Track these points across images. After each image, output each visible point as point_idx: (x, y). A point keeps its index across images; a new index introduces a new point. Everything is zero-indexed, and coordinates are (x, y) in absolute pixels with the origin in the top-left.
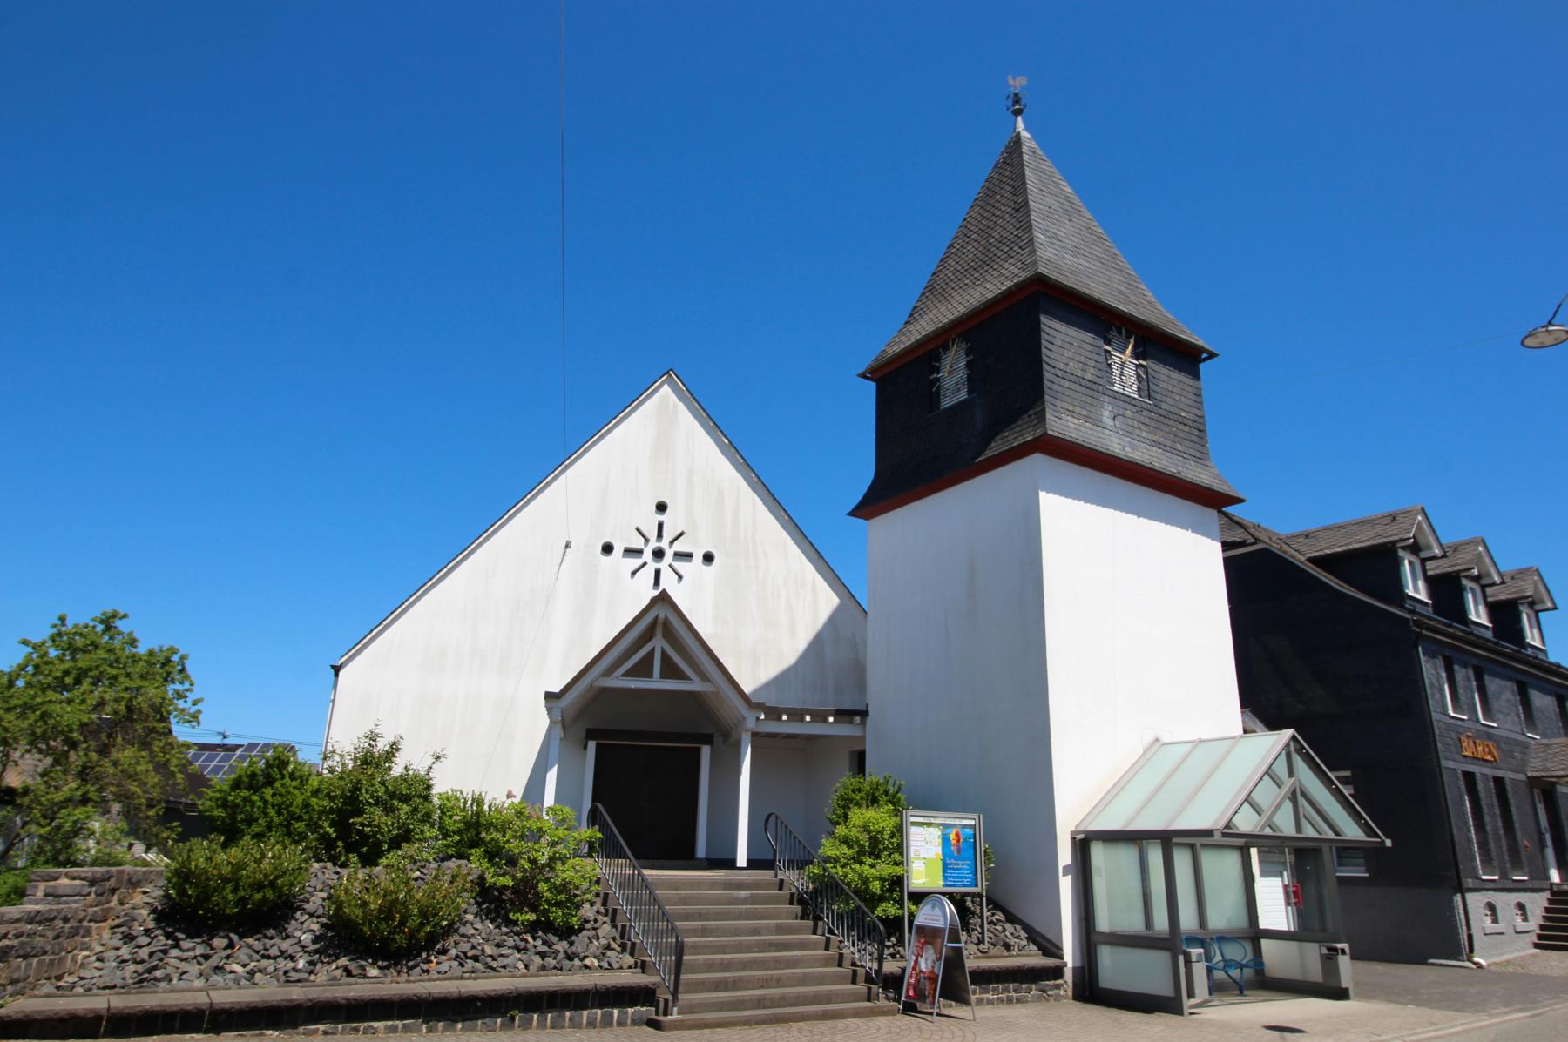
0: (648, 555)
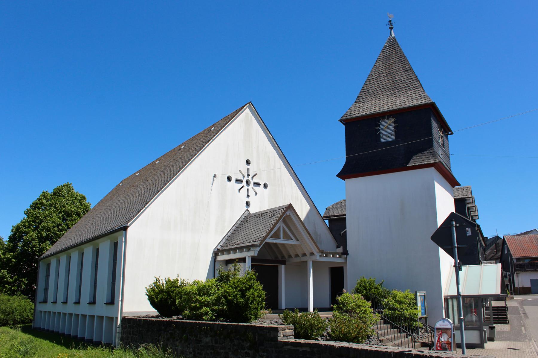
0: (244, 183)
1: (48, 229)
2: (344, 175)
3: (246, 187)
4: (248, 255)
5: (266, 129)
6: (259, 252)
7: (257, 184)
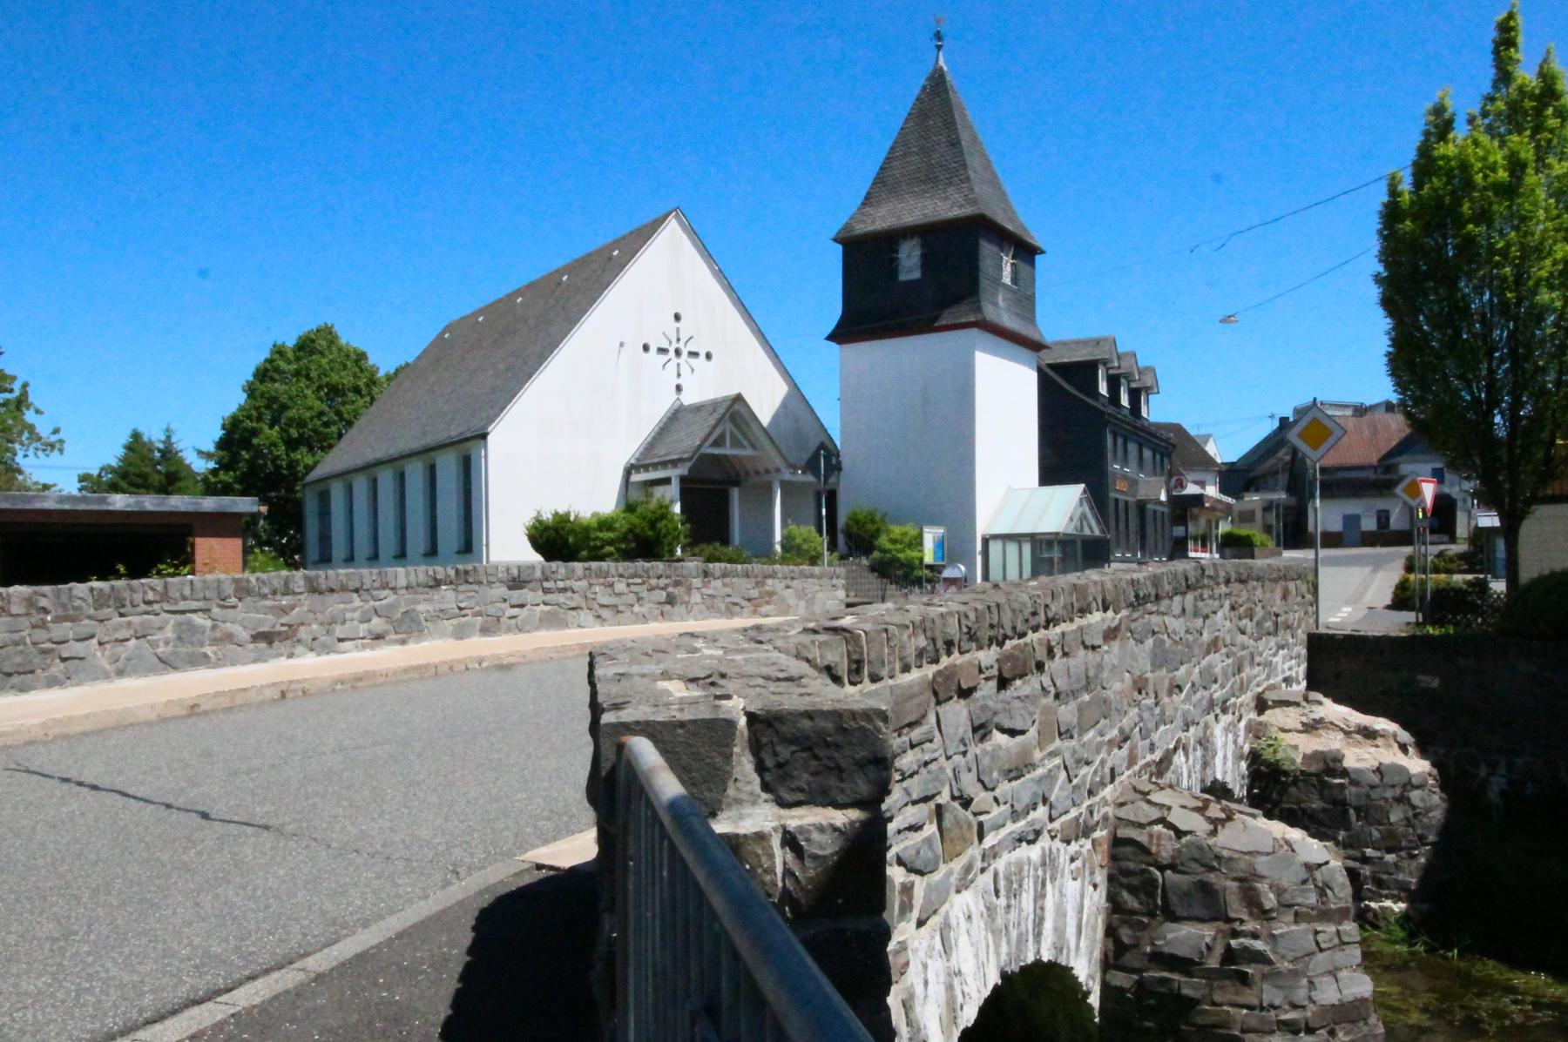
0: (672, 353)
1: (301, 424)
2: (842, 334)
3: (675, 360)
4: (674, 473)
5: (708, 255)
6: (691, 470)
7: (694, 354)
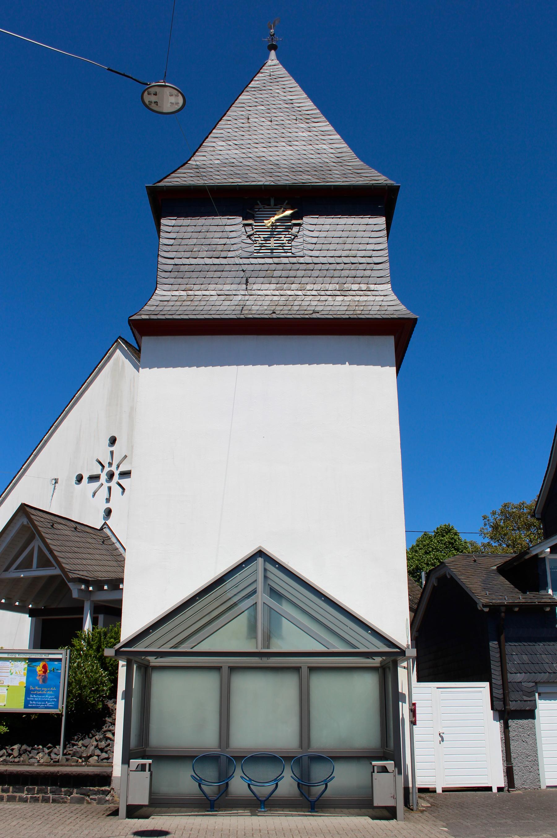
0: (104, 477)
